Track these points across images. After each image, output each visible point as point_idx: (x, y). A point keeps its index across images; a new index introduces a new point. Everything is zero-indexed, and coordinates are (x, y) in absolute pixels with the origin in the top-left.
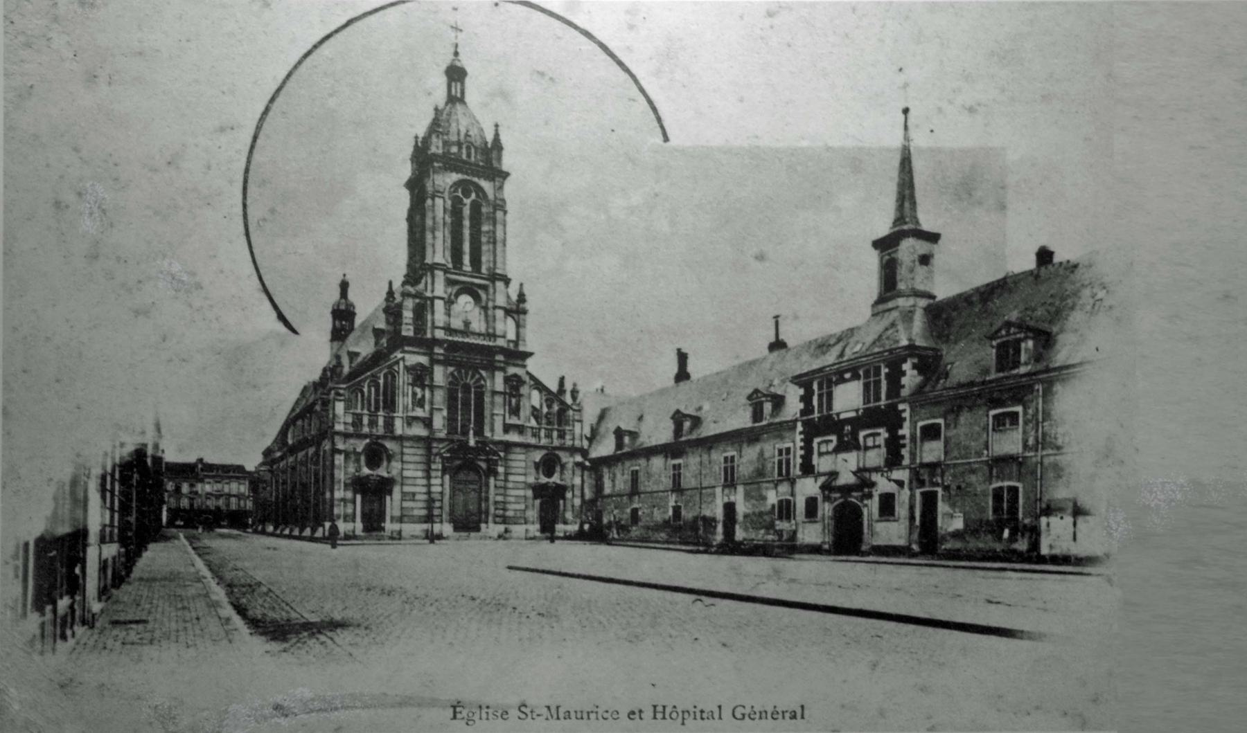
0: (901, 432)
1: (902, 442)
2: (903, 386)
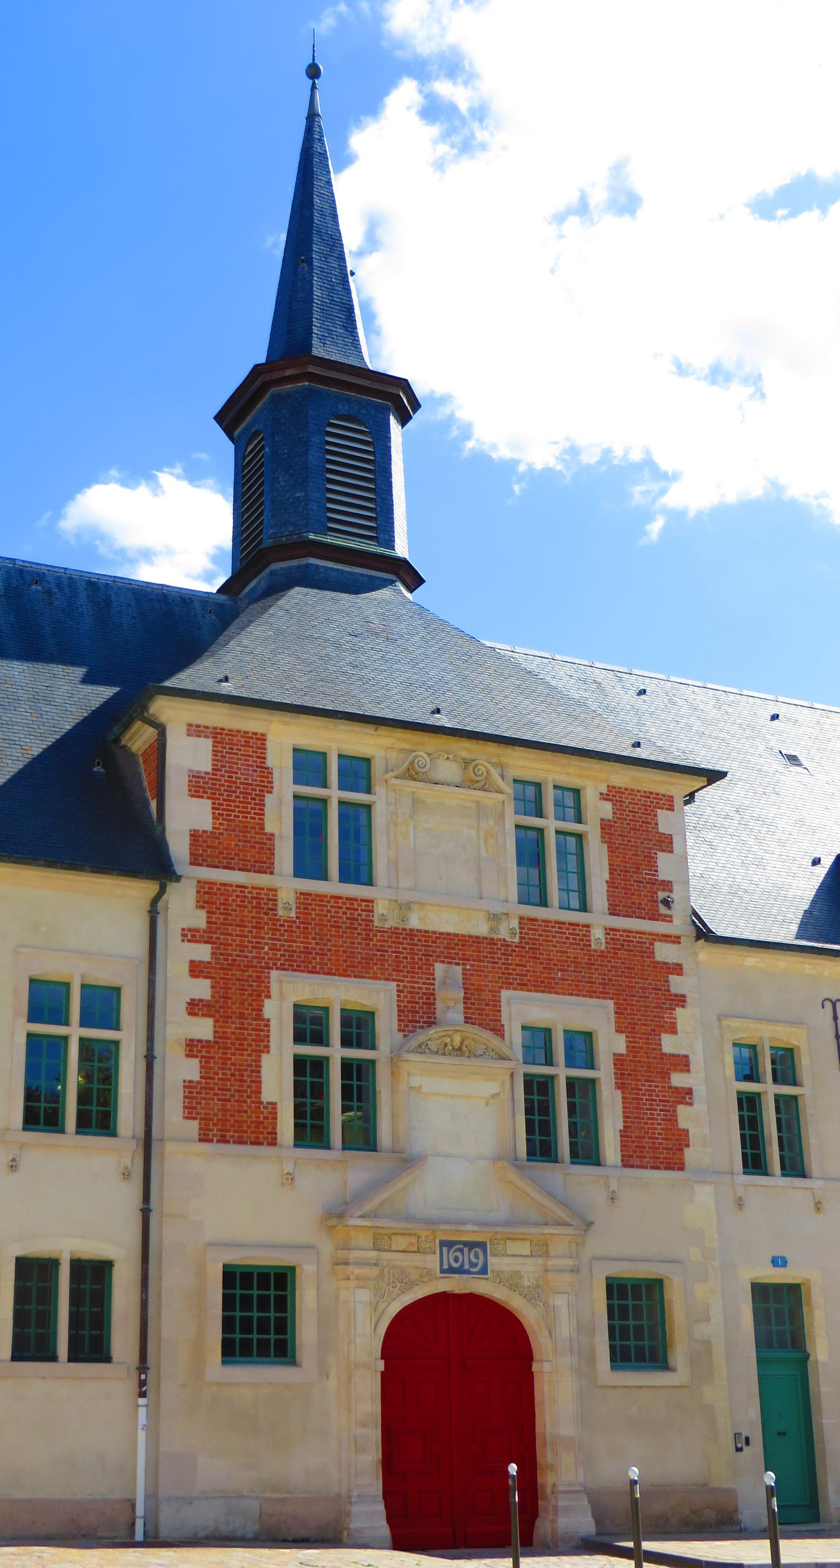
0: (669, 1044)
1: (678, 1080)
2: (672, 1029)
